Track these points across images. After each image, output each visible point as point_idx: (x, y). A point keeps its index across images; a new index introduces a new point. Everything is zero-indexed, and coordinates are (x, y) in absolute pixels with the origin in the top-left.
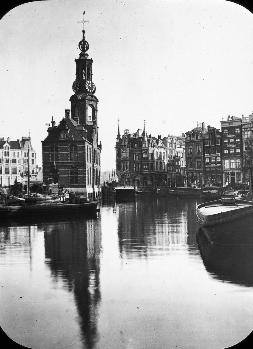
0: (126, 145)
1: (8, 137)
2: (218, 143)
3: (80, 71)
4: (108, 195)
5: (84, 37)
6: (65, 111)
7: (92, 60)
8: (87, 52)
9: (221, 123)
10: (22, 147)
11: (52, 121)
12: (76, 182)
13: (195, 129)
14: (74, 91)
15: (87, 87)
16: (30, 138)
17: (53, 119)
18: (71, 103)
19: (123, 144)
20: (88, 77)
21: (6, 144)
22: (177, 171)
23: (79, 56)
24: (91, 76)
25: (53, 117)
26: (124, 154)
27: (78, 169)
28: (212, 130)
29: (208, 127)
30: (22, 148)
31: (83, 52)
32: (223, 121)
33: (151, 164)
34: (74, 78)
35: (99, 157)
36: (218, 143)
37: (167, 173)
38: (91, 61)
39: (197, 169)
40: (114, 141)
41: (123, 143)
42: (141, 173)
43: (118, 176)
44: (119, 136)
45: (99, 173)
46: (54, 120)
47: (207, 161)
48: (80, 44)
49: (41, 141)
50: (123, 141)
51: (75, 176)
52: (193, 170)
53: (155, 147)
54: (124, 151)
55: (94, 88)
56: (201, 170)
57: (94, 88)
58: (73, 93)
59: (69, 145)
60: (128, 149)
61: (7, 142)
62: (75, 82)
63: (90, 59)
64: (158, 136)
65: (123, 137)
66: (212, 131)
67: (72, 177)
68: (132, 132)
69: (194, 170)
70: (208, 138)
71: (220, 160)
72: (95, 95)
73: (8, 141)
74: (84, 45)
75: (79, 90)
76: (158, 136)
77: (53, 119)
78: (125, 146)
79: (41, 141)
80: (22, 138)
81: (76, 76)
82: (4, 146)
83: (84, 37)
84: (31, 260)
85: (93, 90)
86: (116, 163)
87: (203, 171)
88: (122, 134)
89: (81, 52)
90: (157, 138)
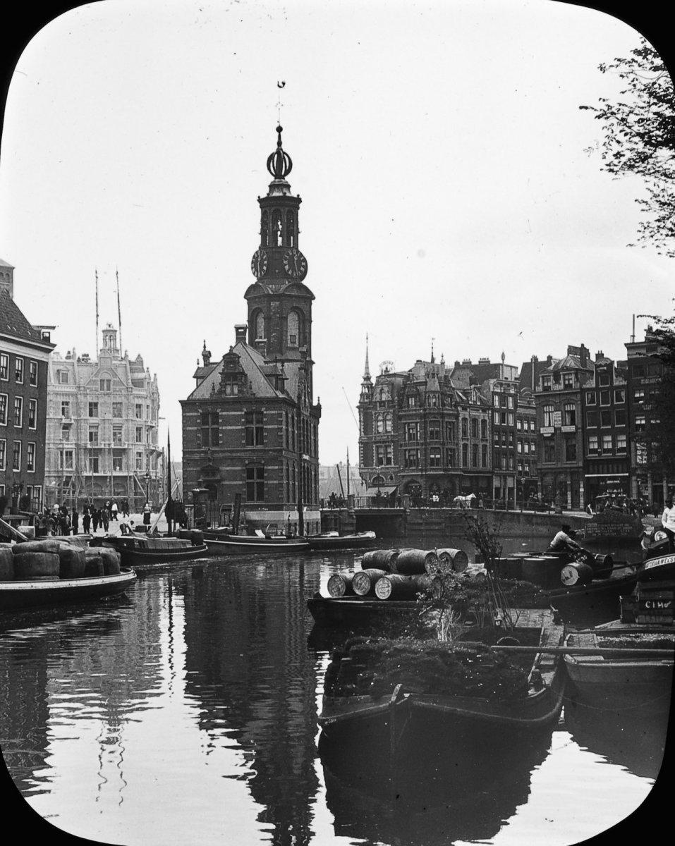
0: (384, 402)
2: (619, 399)
3: (271, 225)
5: (279, 143)
6: (234, 330)
7: (300, 199)
8: (288, 179)
9: (628, 349)
11: (205, 350)
12: (260, 497)
13: (562, 363)
14: (254, 274)
15: (286, 265)
17: (205, 347)
18: (248, 303)
19: (377, 397)
22: (520, 469)
23: (267, 190)
26: (380, 423)
27: (265, 467)
28: (606, 365)
29: (596, 355)
31: (277, 180)
32: (633, 343)
33: (451, 449)
34: (255, 242)
35: (315, 436)
36: (619, 399)
37: (493, 473)
38: (298, 200)
39: (565, 466)
40: (355, 393)
41: (378, 396)
42: (422, 475)
43: (366, 481)
44: (367, 378)
45: (315, 475)
46: (207, 349)
47: (591, 446)
48: (271, 158)
49: (180, 401)
50: (378, 390)
52: (575, 466)
54: (380, 418)
55: (303, 267)
56: (577, 467)
57: (303, 267)
58: (254, 280)
59: (245, 410)
60: (392, 411)
65: (377, 381)
66: (605, 368)
67: (250, 486)
68: (402, 365)
69: (559, 466)
70: (594, 386)
71: (624, 445)
72: (305, 282)
74: (280, 163)
75: (267, 271)
77: (205, 347)
78: (382, 403)
79: (180, 401)
81: (260, 236)
83: (279, 143)
84: (626, 106)
86: (360, 448)
87: (581, 470)
88: (375, 373)
89: (272, 178)
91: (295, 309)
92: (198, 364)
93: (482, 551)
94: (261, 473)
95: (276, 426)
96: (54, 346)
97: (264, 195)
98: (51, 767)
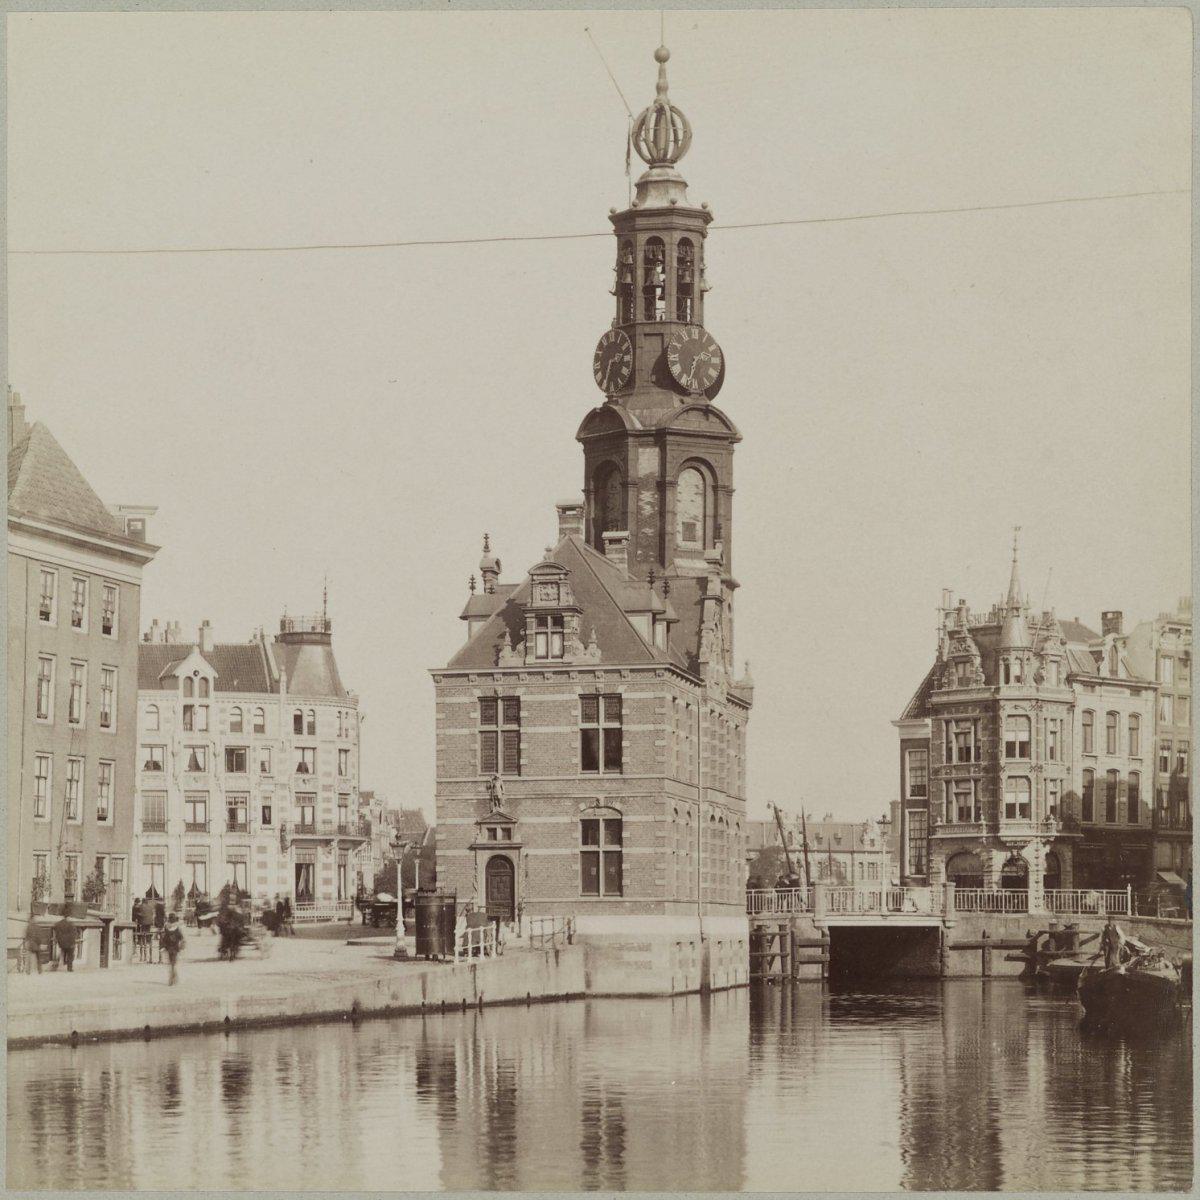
1: (207, 623)
4: (783, 957)
5: (660, 89)
8: (681, 170)
10: (284, 678)
14: (600, 384)
15: (674, 363)
16: (327, 625)
18: (586, 451)
20: (681, 307)
21: (195, 663)
24: (697, 301)
25: (486, 538)
30: (283, 686)
51: (606, 731)
53: (1077, 687)
55: (714, 366)
57: (714, 366)
58: (598, 399)
61: (196, 650)
62: (607, 336)
63: (697, 206)
64: (1105, 614)
72: (717, 403)
73: (200, 646)
76: (1105, 614)
80: (283, 624)
81: (615, 274)
82: (183, 671)
85: (709, 377)
90: (1096, 626)
91: (696, 463)
92: (473, 588)
93: (929, 854)
94: (616, 828)
95: (651, 727)
96: (155, 549)
97: (623, 207)
98: (181, 883)
